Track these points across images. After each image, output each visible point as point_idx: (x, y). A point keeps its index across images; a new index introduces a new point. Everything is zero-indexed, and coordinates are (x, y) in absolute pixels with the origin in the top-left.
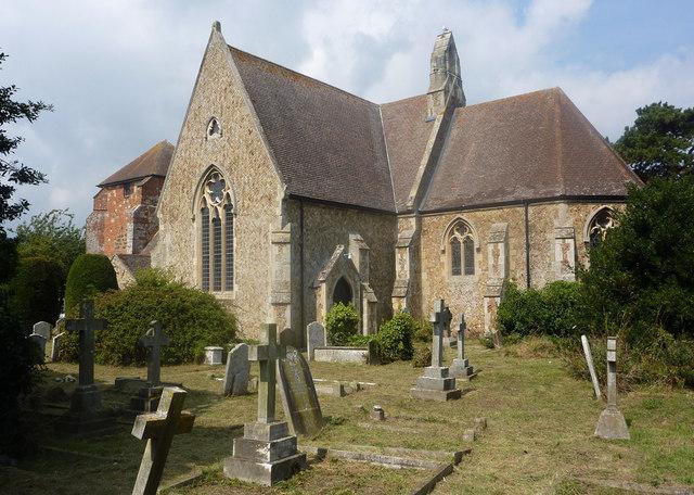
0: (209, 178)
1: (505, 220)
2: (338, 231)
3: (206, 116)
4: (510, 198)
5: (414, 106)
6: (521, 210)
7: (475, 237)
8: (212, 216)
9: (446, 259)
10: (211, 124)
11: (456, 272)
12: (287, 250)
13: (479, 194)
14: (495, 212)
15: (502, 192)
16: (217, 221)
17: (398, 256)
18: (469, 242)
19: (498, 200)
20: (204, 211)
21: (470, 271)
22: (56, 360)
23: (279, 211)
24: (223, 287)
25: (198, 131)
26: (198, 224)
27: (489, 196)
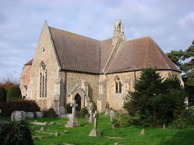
0: (42, 64)
1: (130, 76)
2: (78, 79)
3: (42, 46)
4: (131, 70)
5: (110, 41)
6: (133, 73)
7: (121, 81)
8: (42, 75)
9: (114, 88)
10: (43, 49)
11: (117, 92)
12: (59, 85)
13: (123, 68)
14: (126, 73)
15: (130, 68)
16: (43, 76)
17: (99, 87)
18: (120, 83)
19: (128, 70)
20: (41, 74)
21: (120, 92)
22: (189, 106)
23: (58, 74)
24: (119, 92)
25: (40, 51)
26: (39, 77)
27: (126, 69)
